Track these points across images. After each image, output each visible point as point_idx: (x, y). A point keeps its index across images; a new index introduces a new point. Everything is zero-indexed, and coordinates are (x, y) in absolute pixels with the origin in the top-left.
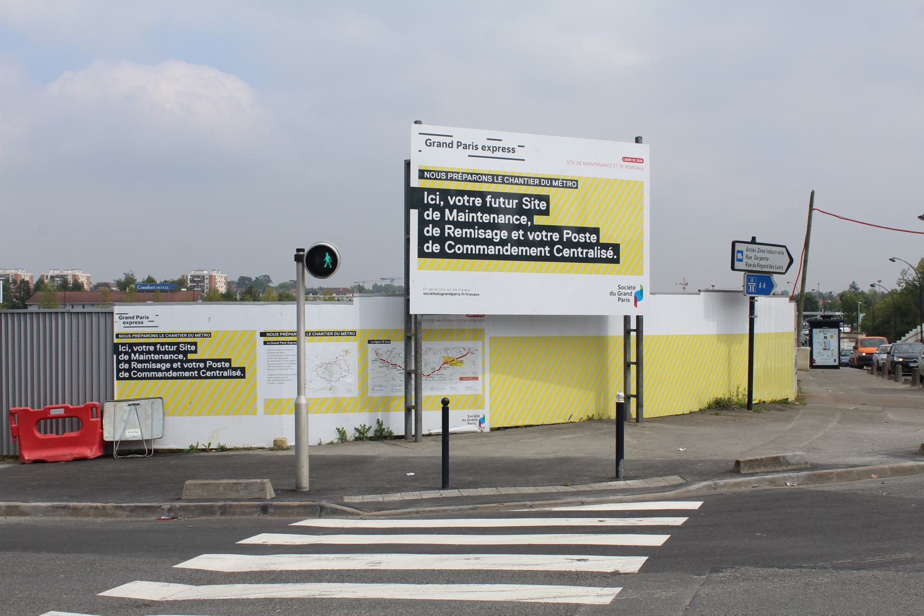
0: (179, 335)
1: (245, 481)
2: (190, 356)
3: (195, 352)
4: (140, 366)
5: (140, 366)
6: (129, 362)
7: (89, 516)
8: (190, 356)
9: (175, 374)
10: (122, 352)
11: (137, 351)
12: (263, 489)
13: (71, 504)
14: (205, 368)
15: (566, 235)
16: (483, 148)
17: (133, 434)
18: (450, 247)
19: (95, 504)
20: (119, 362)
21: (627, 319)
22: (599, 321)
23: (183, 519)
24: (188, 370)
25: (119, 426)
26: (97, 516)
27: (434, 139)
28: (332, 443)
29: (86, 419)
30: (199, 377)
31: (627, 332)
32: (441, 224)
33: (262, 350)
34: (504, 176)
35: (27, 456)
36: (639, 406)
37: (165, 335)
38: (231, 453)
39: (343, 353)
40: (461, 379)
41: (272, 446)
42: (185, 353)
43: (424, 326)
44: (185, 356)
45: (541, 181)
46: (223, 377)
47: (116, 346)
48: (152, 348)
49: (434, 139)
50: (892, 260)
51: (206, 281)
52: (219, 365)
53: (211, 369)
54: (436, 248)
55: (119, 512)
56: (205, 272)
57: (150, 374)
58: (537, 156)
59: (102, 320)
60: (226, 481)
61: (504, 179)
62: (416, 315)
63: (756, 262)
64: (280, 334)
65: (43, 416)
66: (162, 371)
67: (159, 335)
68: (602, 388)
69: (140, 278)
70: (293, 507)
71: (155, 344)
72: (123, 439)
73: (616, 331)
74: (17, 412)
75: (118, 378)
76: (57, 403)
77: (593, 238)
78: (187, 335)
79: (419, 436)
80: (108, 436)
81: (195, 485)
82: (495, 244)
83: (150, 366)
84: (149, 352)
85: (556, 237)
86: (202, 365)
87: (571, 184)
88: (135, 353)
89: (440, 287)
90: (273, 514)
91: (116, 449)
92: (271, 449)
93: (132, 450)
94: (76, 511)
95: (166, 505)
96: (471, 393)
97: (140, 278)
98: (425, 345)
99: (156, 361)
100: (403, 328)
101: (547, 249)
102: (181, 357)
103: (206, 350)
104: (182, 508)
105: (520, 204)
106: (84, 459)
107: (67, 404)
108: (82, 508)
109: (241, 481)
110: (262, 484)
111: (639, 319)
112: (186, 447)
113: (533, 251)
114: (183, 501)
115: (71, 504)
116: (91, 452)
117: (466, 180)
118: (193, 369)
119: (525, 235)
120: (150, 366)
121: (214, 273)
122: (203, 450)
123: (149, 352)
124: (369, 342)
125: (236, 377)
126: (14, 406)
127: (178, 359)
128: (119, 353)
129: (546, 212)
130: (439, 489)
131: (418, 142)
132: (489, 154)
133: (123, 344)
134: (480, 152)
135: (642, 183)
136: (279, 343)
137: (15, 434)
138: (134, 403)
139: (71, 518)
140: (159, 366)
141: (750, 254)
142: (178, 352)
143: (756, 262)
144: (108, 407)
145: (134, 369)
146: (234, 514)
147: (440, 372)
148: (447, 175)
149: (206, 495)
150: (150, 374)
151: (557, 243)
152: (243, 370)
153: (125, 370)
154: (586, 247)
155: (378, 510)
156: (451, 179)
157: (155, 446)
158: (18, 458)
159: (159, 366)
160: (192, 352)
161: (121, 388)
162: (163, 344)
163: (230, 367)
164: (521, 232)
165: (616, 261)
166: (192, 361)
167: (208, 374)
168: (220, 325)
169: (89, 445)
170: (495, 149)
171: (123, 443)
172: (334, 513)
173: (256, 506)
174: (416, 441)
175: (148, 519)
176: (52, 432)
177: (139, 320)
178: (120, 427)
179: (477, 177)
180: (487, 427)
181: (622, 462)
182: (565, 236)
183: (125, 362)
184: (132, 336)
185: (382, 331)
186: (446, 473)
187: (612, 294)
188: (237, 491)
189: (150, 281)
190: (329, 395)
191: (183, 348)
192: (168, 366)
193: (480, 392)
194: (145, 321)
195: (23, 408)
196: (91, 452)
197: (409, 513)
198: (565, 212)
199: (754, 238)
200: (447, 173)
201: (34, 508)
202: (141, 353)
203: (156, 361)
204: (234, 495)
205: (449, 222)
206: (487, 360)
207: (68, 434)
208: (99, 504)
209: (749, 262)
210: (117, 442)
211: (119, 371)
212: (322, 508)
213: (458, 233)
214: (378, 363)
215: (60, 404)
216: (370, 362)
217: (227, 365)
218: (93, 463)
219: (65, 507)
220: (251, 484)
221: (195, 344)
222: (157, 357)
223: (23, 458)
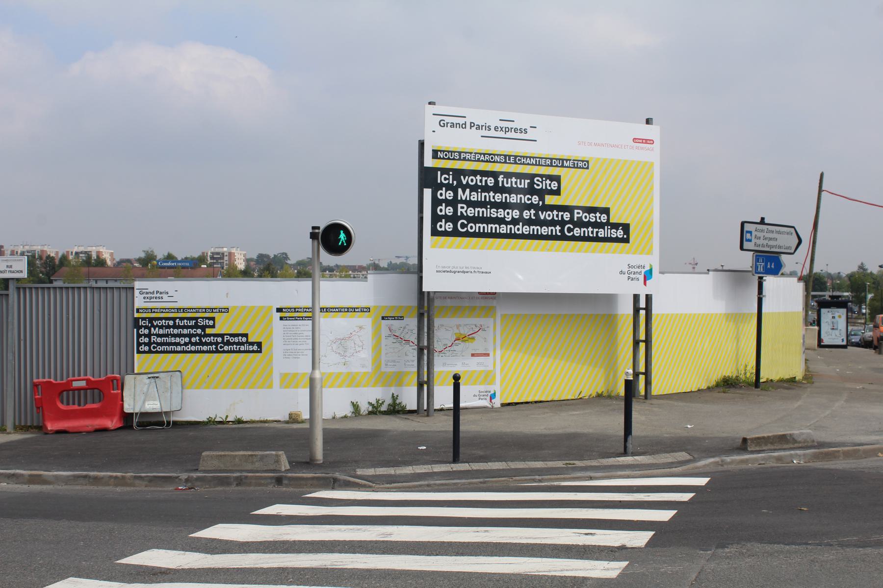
0: (197, 310)
1: (260, 453)
3: (213, 327)
4: (159, 340)
5: (159, 340)
6: (149, 336)
7: (109, 485)
9: (193, 348)
10: (142, 326)
11: (157, 326)
12: (277, 461)
13: (92, 473)
14: (223, 342)
16: (496, 129)
17: (153, 406)
19: (114, 474)
20: (139, 336)
21: (636, 298)
22: (609, 300)
23: (200, 489)
24: (206, 344)
25: (140, 398)
26: (116, 485)
27: (448, 119)
28: (345, 417)
29: (107, 391)
30: (217, 351)
31: (636, 310)
32: (454, 203)
33: (278, 326)
34: (516, 157)
35: (50, 427)
36: (648, 383)
37: (184, 310)
38: (247, 425)
39: (357, 329)
40: (473, 355)
42: (203, 328)
43: (437, 303)
44: (204, 330)
45: (552, 162)
46: (240, 352)
47: (136, 320)
48: (171, 323)
49: (448, 119)
51: (226, 258)
52: (236, 340)
53: (228, 343)
55: (137, 482)
56: (225, 249)
57: (169, 348)
58: (548, 137)
60: (241, 453)
61: (517, 159)
62: (429, 292)
64: (295, 310)
65: (65, 389)
66: (181, 345)
67: (178, 310)
68: (611, 364)
69: (160, 254)
71: (174, 319)
72: (143, 411)
73: (626, 309)
75: (139, 352)
76: (79, 375)
77: (604, 218)
78: (206, 310)
79: (431, 411)
80: (128, 408)
81: (212, 457)
82: (507, 223)
84: (168, 327)
85: (567, 216)
86: (220, 339)
87: (582, 165)
88: (155, 327)
90: (287, 486)
91: (135, 420)
92: (287, 422)
94: (96, 480)
95: (184, 476)
96: (482, 368)
97: (160, 254)
98: (437, 322)
99: (175, 336)
101: (558, 228)
102: (199, 331)
103: (223, 325)
104: (198, 479)
105: (532, 184)
106: (105, 430)
107: (89, 377)
108: (102, 478)
110: (277, 456)
111: (649, 298)
112: (203, 418)
113: (544, 230)
115: (92, 473)
117: (479, 160)
118: (211, 344)
121: (233, 250)
123: (168, 327)
124: (383, 318)
125: (253, 352)
126: (44, 377)
127: (197, 334)
128: (139, 327)
130: (450, 463)
131: (431, 122)
132: (502, 134)
133: (143, 319)
134: (493, 133)
136: (295, 319)
137: (39, 405)
138: (154, 376)
140: (178, 340)
142: (196, 326)
144: (129, 380)
145: (154, 343)
146: (250, 485)
147: (454, 347)
148: (460, 155)
149: (222, 467)
150: (169, 348)
151: (568, 222)
152: (259, 344)
153: (145, 344)
154: (597, 227)
155: (390, 482)
156: (464, 159)
157: (173, 418)
158: (41, 428)
159: (178, 340)
160: (210, 327)
161: (141, 362)
162: (182, 319)
163: (247, 342)
164: (533, 212)
165: (626, 240)
166: (210, 335)
169: (110, 416)
170: (507, 130)
171: (144, 414)
174: (428, 416)
175: (166, 489)
176: (74, 404)
177: (158, 295)
179: (490, 157)
180: (497, 403)
181: (630, 439)
184: (152, 310)
185: (396, 308)
186: (456, 447)
187: (622, 272)
188: (252, 463)
189: (170, 257)
190: (343, 369)
191: (201, 323)
194: (165, 297)
195: (46, 379)
196: (111, 423)
198: (575, 192)
199: (763, 219)
200: (460, 153)
201: (56, 476)
202: (161, 327)
203: (175, 336)
204: (249, 467)
207: (90, 406)
208: (119, 474)
209: (758, 242)
210: (137, 414)
211: (139, 344)
212: (335, 480)
214: (392, 339)
215: (82, 377)
217: (244, 339)
218: (113, 433)
219: (85, 477)
220: (267, 456)
221: (213, 319)
222: (176, 331)
223: (46, 428)
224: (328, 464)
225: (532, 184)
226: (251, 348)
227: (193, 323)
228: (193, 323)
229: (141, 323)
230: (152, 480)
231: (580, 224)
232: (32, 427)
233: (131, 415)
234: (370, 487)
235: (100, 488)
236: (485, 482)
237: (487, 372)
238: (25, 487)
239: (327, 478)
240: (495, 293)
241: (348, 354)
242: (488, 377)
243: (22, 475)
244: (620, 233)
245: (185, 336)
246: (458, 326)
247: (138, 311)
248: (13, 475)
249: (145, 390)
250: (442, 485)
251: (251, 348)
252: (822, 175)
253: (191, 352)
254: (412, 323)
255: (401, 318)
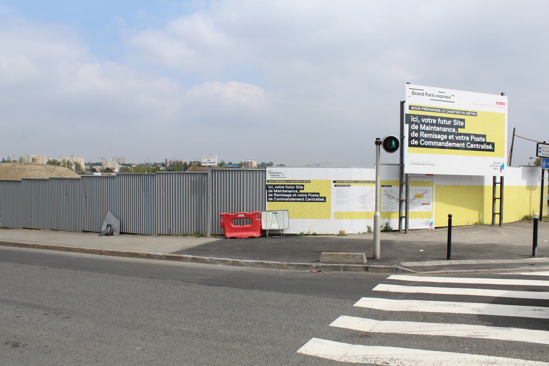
0: (296, 181)
1: (353, 254)
2: (301, 191)
3: (303, 189)
6: (273, 193)
8: (301, 191)
9: (293, 199)
12: (362, 258)
13: (265, 262)
14: (307, 197)
15: (472, 137)
16: (437, 96)
17: (275, 226)
18: (422, 142)
19: (277, 263)
20: (268, 193)
21: (494, 178)
22: (480, 179)
23: (325, 273)
24: (300, 197)
25: (269, 222)
26: (279, 268)
27: (416, 91)
28: (364, 233)
29: (254, 219)
30: (305, 201)
31: (495, 184)
32: (418, 131)
33: (334, 189)
34: (445, 110)
35: (228, 235)
36: (501, 218)
37: (290, 181)
38: (320, 237)
39: (370, 191)
40: (423, 204)
41: (339, 233)
42: (298, 190)
43: (410, 179)
44: (299, 191)
45: (461, 112)
46: (315, 201)
47: (267, 186)
49: (416, 91)
50: (531, 158)
52: (314, 196)
53: (310, 197)
54: (416, 142)
55: (289, 267)
57: (282, 199)
58: (460, 100)
59: (261, 174)
60: (342, 253)
61: (446, 111)
62: (407, 174)
63: (546, 153)
64: (342, 182)
65: (235, 218)
67: (287, 181)
68: (481, 209)
69: (227, 162)
70: (382, 268)
71: (285, 186)
73: (488, 183)
74: (223, 215)
75: (268, 201)
77: (483, 140)
78: (300, 181)
79: (407, 230)
80: (264, 228)
81: (326, 255)
82: (442, 141)
83: (282, 195)
84: (282, 189)
85: (468, 138)
86: (306, 195)
87: (474, 114)
89: (416, 161)
90: (371, 272)
91: (267, 233)
92: (338, 235)
93: (275, 234)
94: (267, 265)
95: (314, 265)
96: (427, 211)
97: (227, 162)
98: (411, 188)
99: (285, 193)
100: (399, 180)
101: (464, 144)
102: (296, 191)
103: (308, 189)
104: (322, 267)
105: (452, 123)
106: (253, 237)
107: (245, 212)
108: (271, 264)
109: (351, 253)
110: (362, 255)
111: (502, 178)
112: (298, 233)
113: (458, 145)
114: (321, 262)
115: (265, 262)
116: (256, 234)
117: (429, 111)
118: (302, 197)
119: (454, 137)
120: (282, 195)
122: (306, 235)
123: (282, 189)
124: (382, 186)
125: (322, 201)
127: (295, 192)
129: (463, 127)
130: (445, 259)
131: (408, 92)
132: (439, 99)
133: (270, 185)
134: (435, 98)
135: (504, 114)
136: (342, 186)
137: (223, 226)
139: (266, 269)
141: (544, 149)
142: (295, 189)
143: (546, 153)
144: (264, 214)
146: (351, 270)
147: (414, 200)
148: (421, 109)
149: (332, 260)
150: (282, 199)
151: (468, 141)
152: (325, 198)
153: (271, 197)
154: (481, 145)
155: (425, 270)
156: (423, 110)
157: (285, 232)
158: (223, 236)
162: (288, 185)
163: (319, 197)
164: (453, 136)
165: (493, 151)
166: (301, 193)
167: (309, 199)
168: (315, 177)
169: (255, 231)
170: (442, 97)
171: (271, 230)
172: (403, 272)
173: (362, 267)
174: (405, 233)
178: (269, 223)
179: (435, 110)
180: (433, 226)
181: (536, 248)
182: (472, 138)
183: (271, 193)
184: (274, 181)
185: (389, 181)
186: (449, 250)
187: (491, 166)
188: (349, 259)
189: (230, 164)
190: (364, 210)
191: (297, 187)
192: (291, 195)
193: (430, 210)
196: (256, 234)
197: (443, 273)
198: (472, 127)
199: (544, 142)
200: (421, 107)
201: (246, 263)
202: (279, 189)
203: (285, 193)
204: (347, 261)
205: (422, 131)
206: (434, 195)
207: (245, 226)
208: (279, 263)
209: (544, 153)
211: (268, 197)
212: (397, 269)
213: (426, 136)
214: (386, 196)
216: (382, 196)
217: (318, 196)
219: (262, 263)
220: (356, 255)
221: (303, 186)
222: (285, 191)
224: (383, 260)
225: (452, 123)
226: (321, 200)
227: (293, 187)
228: (293, 187)
229: (269, 187)
230: (298, 266)
231: (473, 142)
232: (221, 235)
233: (265, 230)
234: (413, 273)
235: (270, 269)
236: (477, 272)
237: (429, 212)
238: (232, 267)
239: (393, 268)
240: (433, 175)
241: (366, 203)
242: (429, 215)
243: (229, 261)
244: (490, 147)
245: (290, 193)
246: (416, 190)
247: (268, 181)
248: (224, 261)
249: (271, 218)
250: (454, 273)
251: (321, 200)
252: (514, 129)
253: (293, 201)
254: (396, 189)
255: (390, 186)
